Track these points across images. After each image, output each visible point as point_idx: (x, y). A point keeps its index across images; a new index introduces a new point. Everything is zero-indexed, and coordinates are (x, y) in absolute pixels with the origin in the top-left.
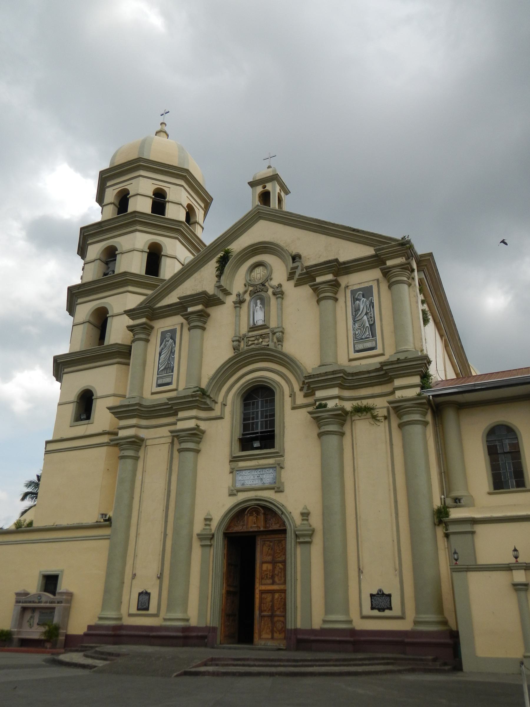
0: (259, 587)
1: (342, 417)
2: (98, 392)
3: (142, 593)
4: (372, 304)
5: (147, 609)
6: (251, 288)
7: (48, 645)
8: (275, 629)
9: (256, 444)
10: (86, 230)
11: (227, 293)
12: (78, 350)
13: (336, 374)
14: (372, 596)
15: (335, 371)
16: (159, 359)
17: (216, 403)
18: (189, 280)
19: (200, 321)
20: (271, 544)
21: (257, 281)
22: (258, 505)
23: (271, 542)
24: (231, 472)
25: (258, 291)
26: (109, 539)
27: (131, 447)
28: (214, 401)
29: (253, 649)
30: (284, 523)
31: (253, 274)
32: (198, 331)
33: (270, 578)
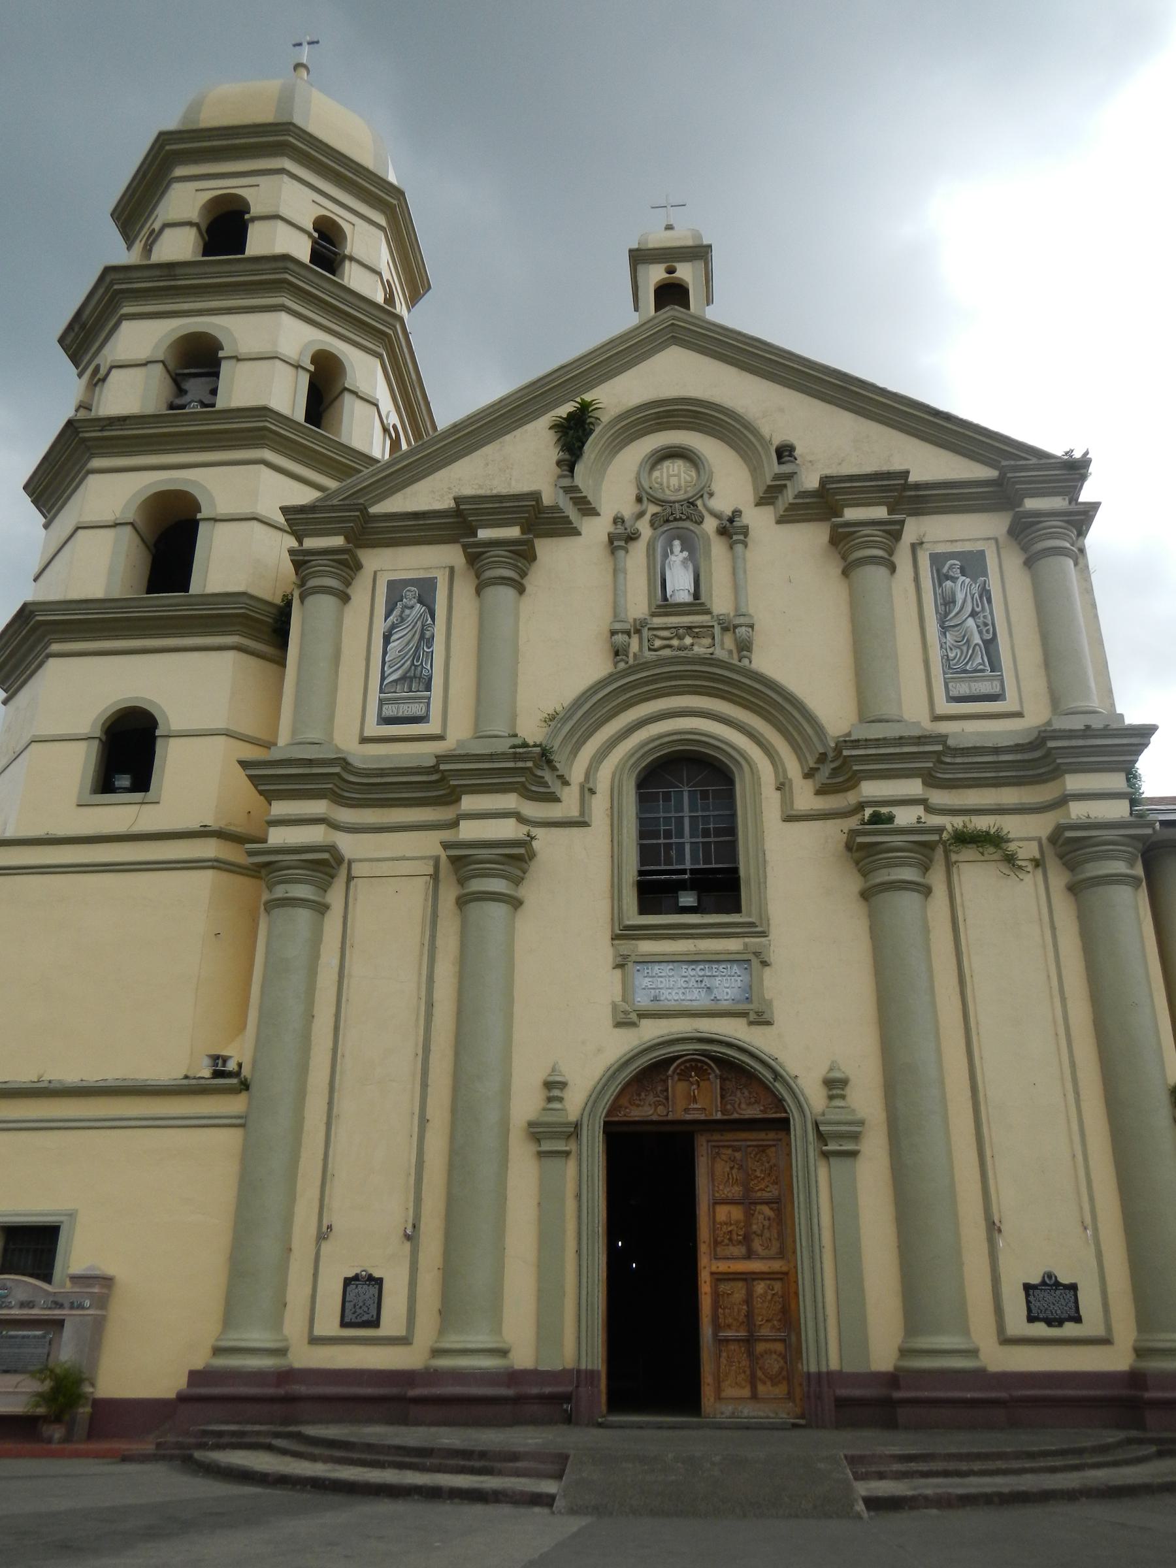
0: (707, 1266)
1: (927, 848)
2: (174, 714)
3: (356, 1278)
4: (985, 593)
5: (375, 1323)
6: (653, 509)
7: (57, 1432)
8: (759, 1373)
9: (687, 899)
10: (121, 275)
11: (587, 509)
12: (100, 594)
13: (925, 744)
14: (1028, 1288)
15: (925, 737)
16: (385, 653)
17: (566, 783)
18: (467, 459)
19: (515, 567)
20: (738, 1155)
21: (668, 492)
22: (704, 1053)
23: (736, 1149)
24: (620, 966)
25: (678, 519)
26: (242, 1126)
27: (274, 878)
28: (561, 777)
29: (700, 1427)
30: (779, 1103)
31: (656, 474)
32: (506, 594)
33: (740, 1242)
